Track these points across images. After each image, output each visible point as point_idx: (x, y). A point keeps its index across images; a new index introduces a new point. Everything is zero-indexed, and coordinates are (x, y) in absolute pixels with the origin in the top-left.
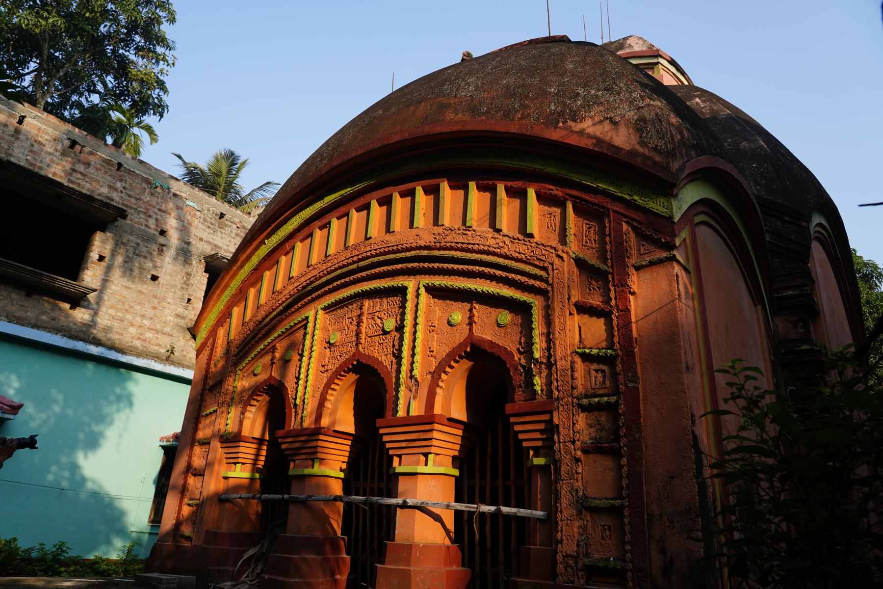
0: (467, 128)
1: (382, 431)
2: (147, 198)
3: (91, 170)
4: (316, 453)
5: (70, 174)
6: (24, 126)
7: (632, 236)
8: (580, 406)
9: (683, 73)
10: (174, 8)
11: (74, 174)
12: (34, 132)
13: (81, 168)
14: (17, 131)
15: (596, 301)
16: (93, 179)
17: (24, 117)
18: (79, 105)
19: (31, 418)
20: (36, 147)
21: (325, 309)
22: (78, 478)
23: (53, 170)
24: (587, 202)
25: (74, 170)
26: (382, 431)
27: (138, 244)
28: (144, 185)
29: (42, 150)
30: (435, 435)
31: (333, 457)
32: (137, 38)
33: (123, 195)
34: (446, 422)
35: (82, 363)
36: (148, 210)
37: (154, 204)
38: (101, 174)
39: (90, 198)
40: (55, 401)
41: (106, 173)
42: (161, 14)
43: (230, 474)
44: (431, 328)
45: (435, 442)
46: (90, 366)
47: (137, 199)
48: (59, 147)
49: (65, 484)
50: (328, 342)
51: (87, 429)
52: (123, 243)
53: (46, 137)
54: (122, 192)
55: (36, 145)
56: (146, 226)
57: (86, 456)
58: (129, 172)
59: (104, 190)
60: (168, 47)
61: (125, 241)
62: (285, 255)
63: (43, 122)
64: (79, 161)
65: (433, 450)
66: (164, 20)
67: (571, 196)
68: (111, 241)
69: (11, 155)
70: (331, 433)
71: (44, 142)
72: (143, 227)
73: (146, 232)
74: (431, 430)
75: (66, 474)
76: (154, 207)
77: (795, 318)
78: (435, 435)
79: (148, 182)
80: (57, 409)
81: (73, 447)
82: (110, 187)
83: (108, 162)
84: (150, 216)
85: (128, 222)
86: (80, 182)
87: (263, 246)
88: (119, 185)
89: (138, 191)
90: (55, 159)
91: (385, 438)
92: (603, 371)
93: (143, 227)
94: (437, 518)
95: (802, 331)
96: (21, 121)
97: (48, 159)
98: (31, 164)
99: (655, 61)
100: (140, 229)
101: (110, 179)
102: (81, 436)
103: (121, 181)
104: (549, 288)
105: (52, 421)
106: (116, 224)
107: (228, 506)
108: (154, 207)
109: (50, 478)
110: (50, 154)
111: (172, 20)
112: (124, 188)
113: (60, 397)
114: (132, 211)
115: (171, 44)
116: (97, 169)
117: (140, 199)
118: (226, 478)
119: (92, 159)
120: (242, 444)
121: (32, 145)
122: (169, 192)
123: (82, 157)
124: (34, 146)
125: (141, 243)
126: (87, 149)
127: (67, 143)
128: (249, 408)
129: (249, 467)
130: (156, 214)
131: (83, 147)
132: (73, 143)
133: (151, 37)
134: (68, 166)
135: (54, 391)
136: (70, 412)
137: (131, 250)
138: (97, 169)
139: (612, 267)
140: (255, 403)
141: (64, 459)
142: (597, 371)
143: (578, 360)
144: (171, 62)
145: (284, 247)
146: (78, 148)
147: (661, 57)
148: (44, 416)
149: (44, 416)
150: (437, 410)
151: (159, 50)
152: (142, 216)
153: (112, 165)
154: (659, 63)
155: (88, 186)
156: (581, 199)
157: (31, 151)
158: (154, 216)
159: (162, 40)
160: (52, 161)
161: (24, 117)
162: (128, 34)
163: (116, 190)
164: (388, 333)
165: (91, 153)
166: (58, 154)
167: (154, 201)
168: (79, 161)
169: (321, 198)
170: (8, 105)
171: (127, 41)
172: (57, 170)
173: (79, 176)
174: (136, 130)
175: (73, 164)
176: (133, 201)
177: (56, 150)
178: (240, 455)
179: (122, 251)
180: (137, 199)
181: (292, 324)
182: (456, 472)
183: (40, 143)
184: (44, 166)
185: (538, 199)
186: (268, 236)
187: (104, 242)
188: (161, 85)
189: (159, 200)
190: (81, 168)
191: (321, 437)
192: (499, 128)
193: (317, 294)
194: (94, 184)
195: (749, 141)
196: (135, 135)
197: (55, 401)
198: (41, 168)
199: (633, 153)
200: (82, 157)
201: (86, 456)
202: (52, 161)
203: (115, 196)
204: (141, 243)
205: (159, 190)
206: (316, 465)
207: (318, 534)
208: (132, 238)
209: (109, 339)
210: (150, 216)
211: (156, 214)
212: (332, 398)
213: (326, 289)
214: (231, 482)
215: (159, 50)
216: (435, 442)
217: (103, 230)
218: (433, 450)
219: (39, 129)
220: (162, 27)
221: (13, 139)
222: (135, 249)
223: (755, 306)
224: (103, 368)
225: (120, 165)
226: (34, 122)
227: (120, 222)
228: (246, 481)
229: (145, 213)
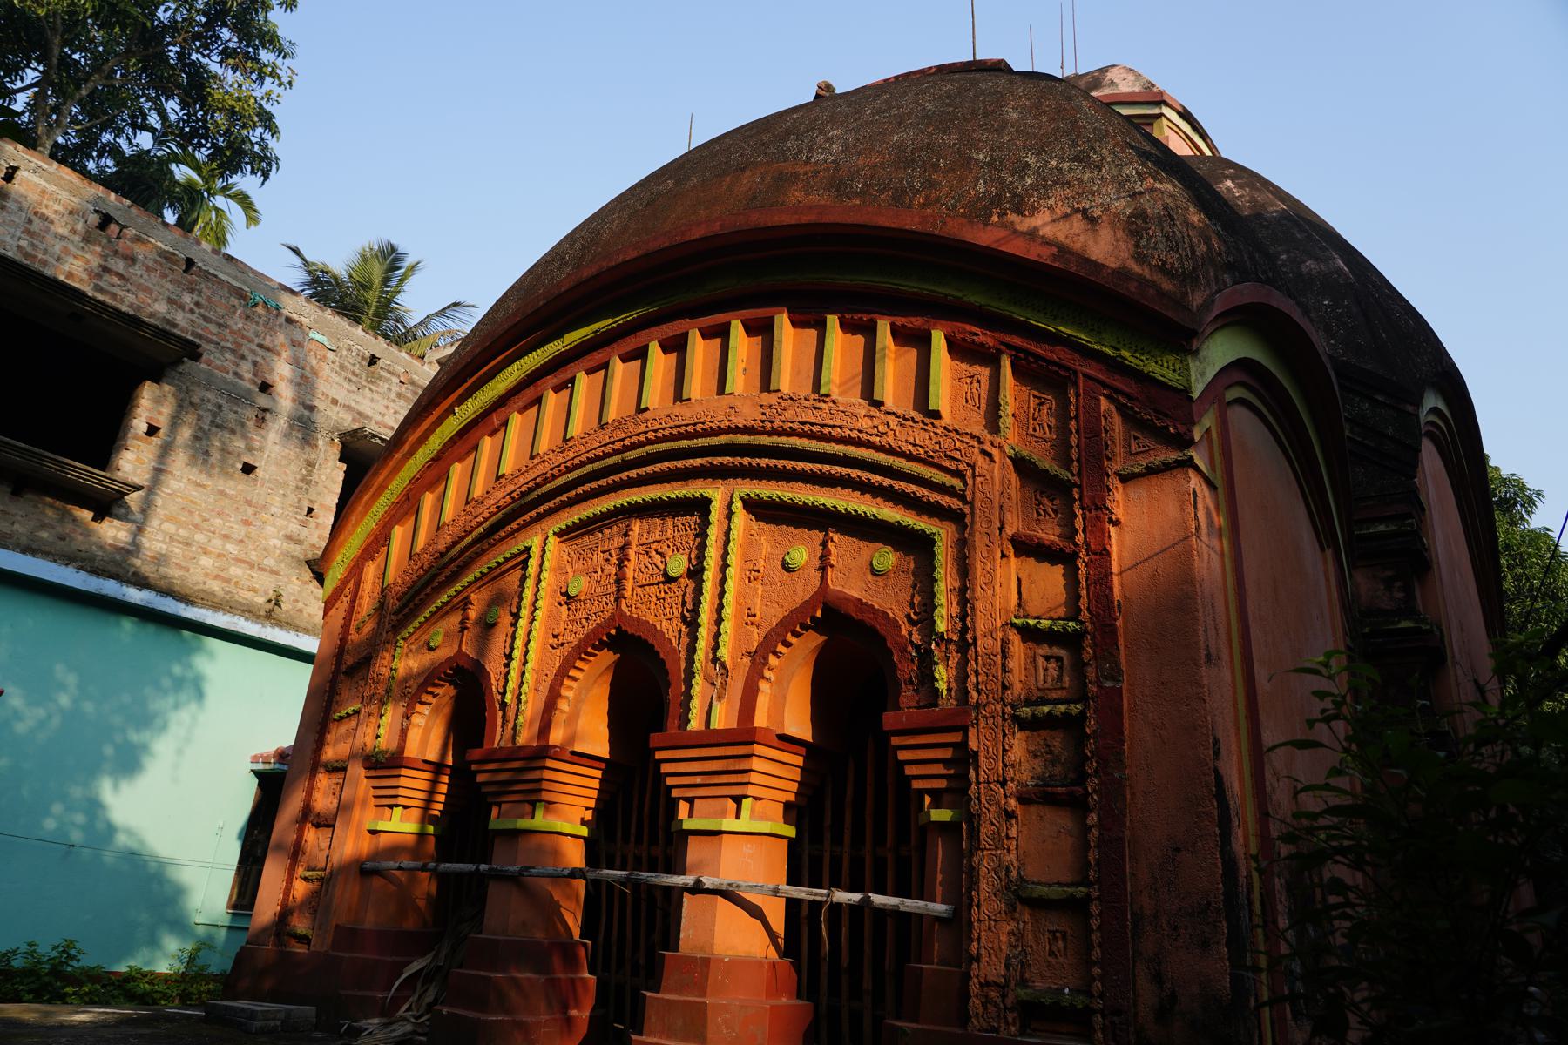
1: (659, 755)
2: (237, 323)
3: (137, 270)
4: (540, 790)
5: (99, 276)
6: (16, 186)
7: (1117, 420)
9: (1204, 136)
11: (106, 277)
12: (33, 197)
15: (1049, 533)
16: (139, 287)
17: (15, 169)
18: (114, 151)
19: (17, 715)
20: (37, 225)
21: (560, 534)
22: (100, 826)
24: (1037, 357)
25: (106, 269)
26: (659, 755)
27: (220, 407)
28: (234, 301)
29: (47, 230)
30: (756, 764)
31: (569, 799)
32: (225, 34)
33: (194, 317)
34: (776, 742)
35: (112, 618)
36: (239, 345)
37: (250, 335)
38: (155, 277)
39: (134, 321)
40: (62, 687)
41: (164, 276)
43: (381, 826)
44: (753, 574)
45: (754, 778)
46: (128, 624)
47: (220, 325)
48: (80, 226)
49: (76, 836)
50: (566, 594)
51: (118, 738)
52: (192, 404)
53: (56, 207)
54: (192, 311)
55: (36, 220)
57: (116, 787)
58: (207, 276)
59: (161, 308)
60: (282, 52)
61: (196, 400)
62: (491, 435)
63: (58, 181)
65: (751, 790)
67: (1009, 346)
68: (171, 399)
70: (568, 756)
71: (52, 216)
72: (230, 377)
73: (235, 385)
75: (80, 818)
76: (251, 341)
77: (1389, 573)
79: (240, 294)
80: (64, 700)
81: (92, 770)
82: (171, 301)
83: (168, 257)
84: (243, 357)
86: (117, 290)
87: (451, 418)
88: (187, 299)
89: (221, 311)
90: (71, 247)
91: (665, 768)
92: (1059, 659)
93: (230, 377)
94: (755, 912)
95: (1400, 595)
97: (57, 248)
98: (27, 255)
99: (1156, 111)
101: (171, 287)
102: (109, 750)
103: (191, 291)
104: (967, 509)
105: (56, 721)
106: (181, 368)
107: (377, 882)
108: (251, 341)
109: (50, 824)
110: (62, 238)
112: (197, 304)
113: (72, 679)
114: (211, 347)
115: (286, 46)
117: (225, 326)
118: (374, 832)
119: (140, 251)
120: (404, 772)
121: (30, 221)
122: (279, 314)
123: (121, 245)
124: (34, 223)
125: (226, 406)
126: (131, 232)
127: (94, 219)
128: (419, 708)
130: (255, 353)
131: (123, 227)
132: (106, 220)
134: (95, 262)
135: (60, 670)
136: (89, 707)
137: (208, 418)
138: (148, 269)
139: (1079, 474)
140: (429, 698)
141: (77, 792)
142: (1047, 658)
143: (1014, 637)
144: (285, 80)
145: (490, 420)
146: (114, 228)
148: (41, 712)
149: (41, 712)
150: (760, 720)
151: (265, 56)
152: (227, 355)
153: (176, 262)
154: (1162, 115)
155: (131, 298)
156: (1028, 352)
157: (28, 232)
158: (251, 357)
159: (270, 39)
160: (66, 251)
161: (15, 169)
162: (209, 25)
163: (182, 307)
164: (674, 580)
165: (137, 239)
166: (77, 238)
167: (252, 327)
168: (116, 252)
169: (558, 335)
171: (207, 39)
172: (74, 268)
173: (115, 280)
174: (220, 201)
175: (105, 257)
176: (213, 328)
177: (73, 231)
178: (401, 792)
179: (190, 418)
180: (220, 325)
181: (501, 560)
182: (791, 831)
184: (51, 260)
186: (461, 401)
187: (157, 401)
188: (267, 121)
189: (261, 329)
190: (119, 265)
191: (549, 763)
193: (546, 506)
194: (142, 295)
195: (1318, 259)
196: (217, 210)
197: (62, 687)
198: (45, 263)
199: (1122, 274)
200: (121, 245)
201: (116, 787)
202: (66, 251)
203: (180, 318)
204: (226, 406)
205: (260, 310)
206: (539, 813)
207: (539, 936)
208: (209, 395)
209: (163, 577)
210: (243, 357)
211: (255, 353)
213: (564, 497)
214: (384, 840)
215: (265, 56)
216: (754, 778)
217: (157, 380)
219: (43, 192)
222: (215, 415)
224: (151, 629)
225: (190, 263)
226: (35, 179)
227: (188, 365)
228: (411, 839)
229: (233, 351)
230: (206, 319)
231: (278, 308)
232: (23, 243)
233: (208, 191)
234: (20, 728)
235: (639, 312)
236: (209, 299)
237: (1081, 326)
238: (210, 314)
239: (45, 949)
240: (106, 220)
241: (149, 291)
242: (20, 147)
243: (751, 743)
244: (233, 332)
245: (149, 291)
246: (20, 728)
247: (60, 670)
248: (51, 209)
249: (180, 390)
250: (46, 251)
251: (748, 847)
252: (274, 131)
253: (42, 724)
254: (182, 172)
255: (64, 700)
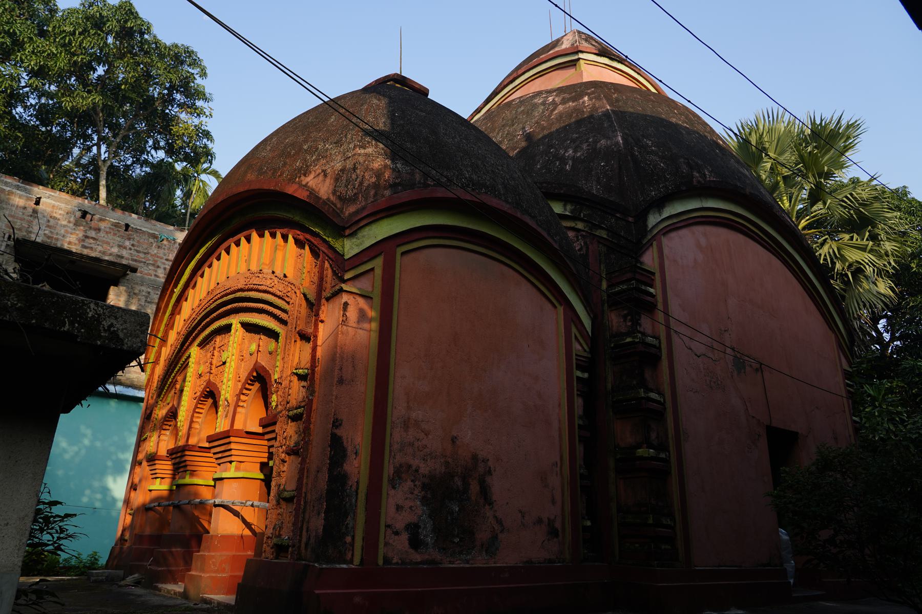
0: (252, 187)
2: (154, 251)
3: (102, 234)
4: (186, 466)
5: (83, 241)
6: (41, 207)
7: (330, 271)
8: (289, 417)
10: (204, 63)
11: (87, 240)
12: (49, 210)
13: (92, 234)
14: (35, 211)
16: (104, 242)
17: (40, 198)
18: (146, 162)
19: (65, 451)
20: (52, 222)
22: (109, 499)
23: (68, 240)
25: (87, 237)
28: (151, 240)
29: (57, 224)
30: (233, 446)
31: (204, 469)
32: (178, 96)
33: (132, 252)
34: (245, 435)
36: (156, 261)
37: (161, 255)
38: (110, 236)
40: (84, 436)
41: (115, 234)
42: (193, 71)
43: (152, 488)
45: (233, 452)
46: (113, 403)
47: (145, 253)
48: (72, 219)
49: (98, 505)
51: (114, 458)
52: (135, 294)
54: (130, 249)
55: (51, 220)
56: (156, 276)
57: (115, 480)
58: (137, 230)
59: (115, 250)
60: (206, 99)
61: (136, 291)
64: (90, 228)
65: (233, 458)
66: (196, 77)
68: (124, 293)
69: (31, 232)
71: (59, 217)
72: (153, 277)
73: (155, 281)
74: (230, 443)
75: (99, 496)
76: (162, 258)
78: (233, 446)
79: (154, 236)
80: (86, 442)
82: (119, 246)
83: (116, 225)
84: (158, 267)
85: (138, 274)
88: (127, 243)
89: (145, 246)
90: (69, 230)
93: (153, 277)
94: (236, 514)
95: (629, 324)
96: (38, 202)
97: (62, 232)
98: (49, 237)
99: (576, 57)
100: (150, 280)
101: (119, 239)
102: (110, 464)
103: (129, 239)
105: (83, 452)
106: (128, 277)
108: (162, 258)
109: (85, 500)
110: (65, 226)
111: (204, 74)
112: (133, 245)
113: (89, 432)
114: (142, 264)
115: (208, 95)
116: (107, 233)
118: (150, 491)
119: (102, 225)
120: (157, 462)
121: (49, 221)
122: (175, 243)
123: (93, 224)
126: (97, 217)
127: (79, 214)
128: (163, 432)
129: (168, 481)
130: (164, 264)
131: (93, 215)
132: (84, 214)
133: (193, 95)
134: (81, 234)
135: (83, 429)
136: (98, 444)
138: (107, 233)
140: (167, 427)
141: (96, 484)
143: (295, 379)
144: (207, 113)
145: (182, 297)
146: (89, 217)
147: (582, 52)
148: (75, 448)
149: (75, 448)
151: (199, 103)
152: (150, 267)
153: (120, 227)
154: (579, 59)
155: (100, 248)
157: (48, 226)
158: (162, 266)
159: (201, 94)
160: (67, 232)
161: (40, 198)
162: (170, 94)
163: (125, 248)
165: (101, 220)
166: (71, 225)
167: (161, 252)
168: (90, 228)
169: (198, 252)
170: (25, 190)
171: (171, 101)
172: (71, 241)
173: (92, 241)
174: (203, 177)
176: (142, 255)
177: (69, 222)
178: (157, 471)
180: (145, 253)
183: (55, 218)
185: (296, 244)
186: (176, 286)
187: (118, 295)
188: (207, 135)
189: (166, 251)
190: (92, 234)
191: (187, 453)
192: (265, 188)
194: (105, 246)
195: (608, 138)
196: (202, 181)
197: (84, 436)
198: (57, 239)
199: (326, 202)
200: (93, 224)
201: (115, 480)
202: (67, 232)
203: (125, 253)
205: (165, 242)
206: (187, 477)
208: (143, 288)
209: (128, 379)
210: (158, 267)
211: (164, 264)
212: (199, 420)
214: (154, 494)
215: (199, 103)
216: (233, 452)
217: (116, 285)
218: (233, 458)
219: (53, 206)
220: (196, 82)
221: (31, 219)
222: (147, 297)
223: (555, 307)
224: (124, 405)
225: (127, 226)
226: (49, 201)
227: (131, 275)
228: (165, 493)
229: (153, 265)
230: (138, 252)
231: (174, 240)
232: (47, 232)
233: (197, 172)
234: (67, 456)
235: (214, 239)
236: (138, 242)
237: (323, 229)
238: (140, 249)
239: (85, 557)
240: (84, 214)
241: (108, 243)
242: (41, 187)
243: (229, 437)
244: (152, 255)
245: (108, 243)
246: (67, 456)
247: (83, 429)
248: (58, 214)
249: (128, 287)
250: (57, 234)
251: (235, 484)
252: (212, 140)
253: (77, 453)
254: (179, 167)
255: (86, 442)
